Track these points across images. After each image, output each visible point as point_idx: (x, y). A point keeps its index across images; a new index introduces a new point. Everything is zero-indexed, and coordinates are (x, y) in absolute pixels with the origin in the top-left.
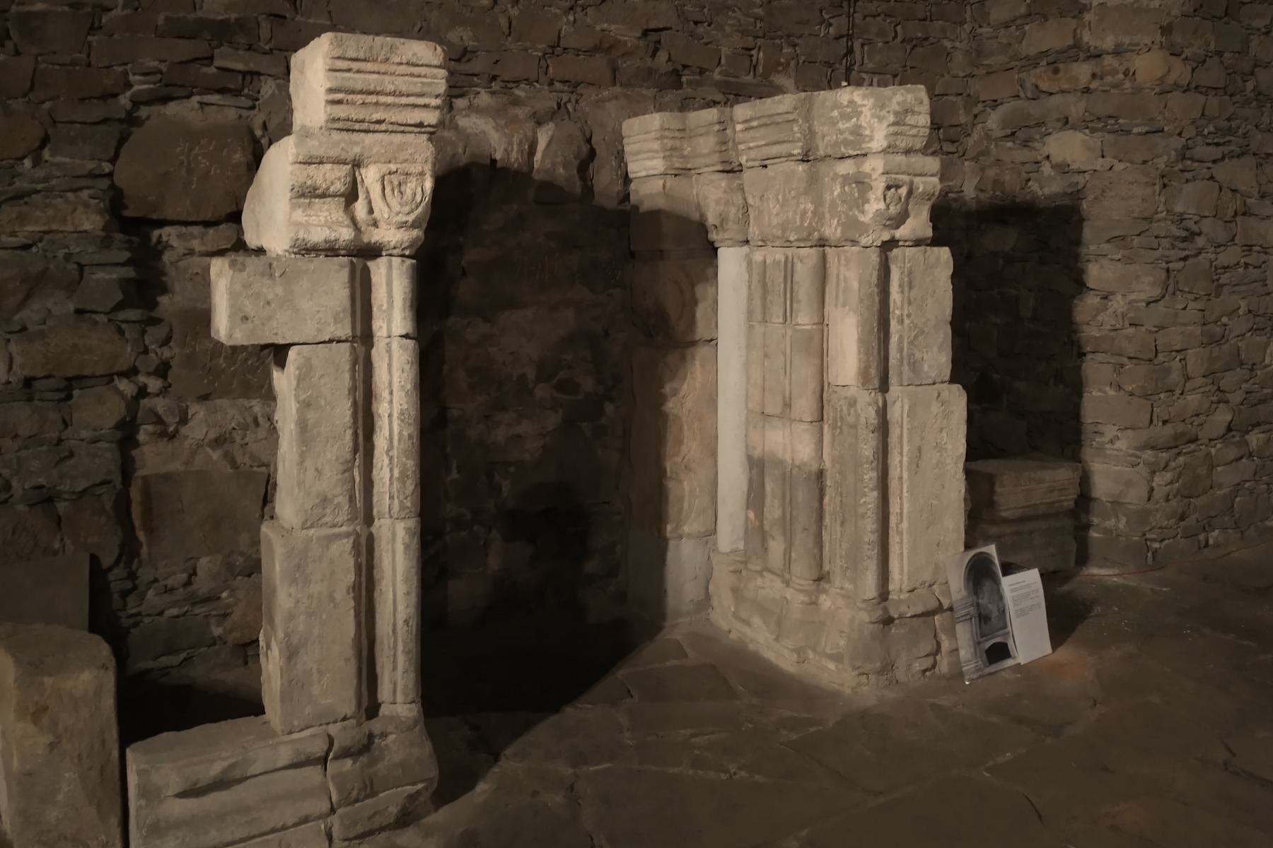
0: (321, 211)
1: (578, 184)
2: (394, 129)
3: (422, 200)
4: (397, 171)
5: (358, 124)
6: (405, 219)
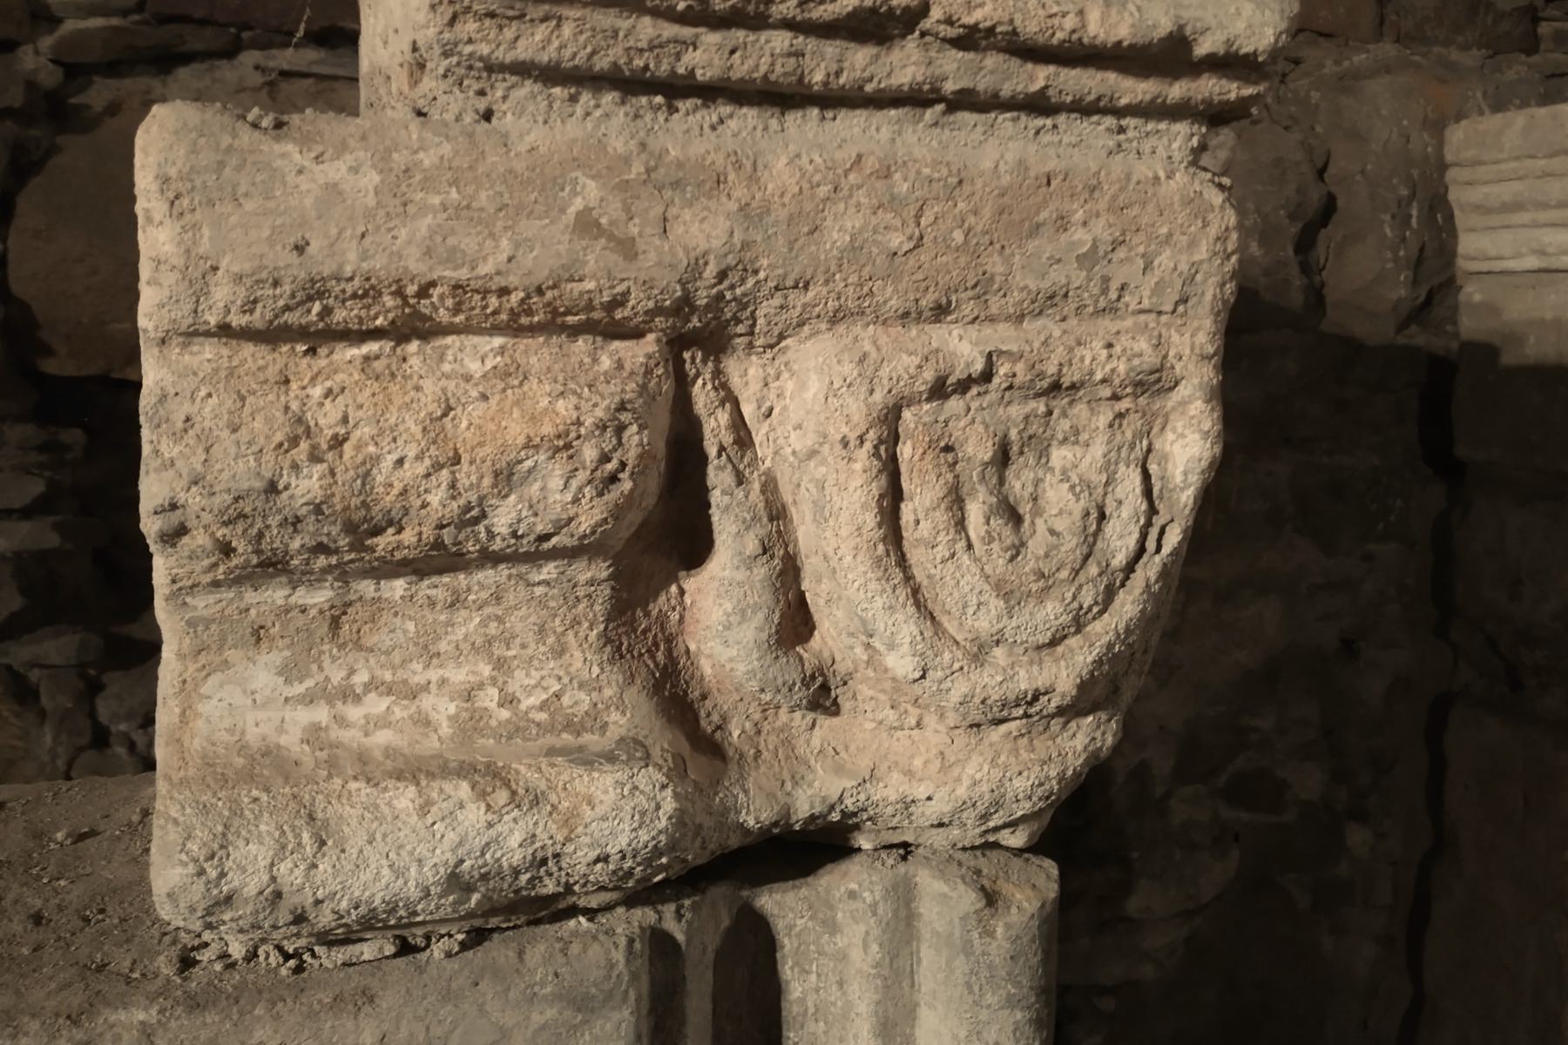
0: (431, 657)
1: (1298, 281)
2: (983, 84)
3: (1141, 550)
4: (987, 376)
5: (711, 38)
6: (1024, 682)
